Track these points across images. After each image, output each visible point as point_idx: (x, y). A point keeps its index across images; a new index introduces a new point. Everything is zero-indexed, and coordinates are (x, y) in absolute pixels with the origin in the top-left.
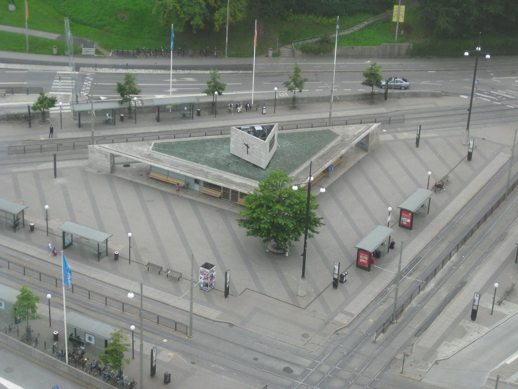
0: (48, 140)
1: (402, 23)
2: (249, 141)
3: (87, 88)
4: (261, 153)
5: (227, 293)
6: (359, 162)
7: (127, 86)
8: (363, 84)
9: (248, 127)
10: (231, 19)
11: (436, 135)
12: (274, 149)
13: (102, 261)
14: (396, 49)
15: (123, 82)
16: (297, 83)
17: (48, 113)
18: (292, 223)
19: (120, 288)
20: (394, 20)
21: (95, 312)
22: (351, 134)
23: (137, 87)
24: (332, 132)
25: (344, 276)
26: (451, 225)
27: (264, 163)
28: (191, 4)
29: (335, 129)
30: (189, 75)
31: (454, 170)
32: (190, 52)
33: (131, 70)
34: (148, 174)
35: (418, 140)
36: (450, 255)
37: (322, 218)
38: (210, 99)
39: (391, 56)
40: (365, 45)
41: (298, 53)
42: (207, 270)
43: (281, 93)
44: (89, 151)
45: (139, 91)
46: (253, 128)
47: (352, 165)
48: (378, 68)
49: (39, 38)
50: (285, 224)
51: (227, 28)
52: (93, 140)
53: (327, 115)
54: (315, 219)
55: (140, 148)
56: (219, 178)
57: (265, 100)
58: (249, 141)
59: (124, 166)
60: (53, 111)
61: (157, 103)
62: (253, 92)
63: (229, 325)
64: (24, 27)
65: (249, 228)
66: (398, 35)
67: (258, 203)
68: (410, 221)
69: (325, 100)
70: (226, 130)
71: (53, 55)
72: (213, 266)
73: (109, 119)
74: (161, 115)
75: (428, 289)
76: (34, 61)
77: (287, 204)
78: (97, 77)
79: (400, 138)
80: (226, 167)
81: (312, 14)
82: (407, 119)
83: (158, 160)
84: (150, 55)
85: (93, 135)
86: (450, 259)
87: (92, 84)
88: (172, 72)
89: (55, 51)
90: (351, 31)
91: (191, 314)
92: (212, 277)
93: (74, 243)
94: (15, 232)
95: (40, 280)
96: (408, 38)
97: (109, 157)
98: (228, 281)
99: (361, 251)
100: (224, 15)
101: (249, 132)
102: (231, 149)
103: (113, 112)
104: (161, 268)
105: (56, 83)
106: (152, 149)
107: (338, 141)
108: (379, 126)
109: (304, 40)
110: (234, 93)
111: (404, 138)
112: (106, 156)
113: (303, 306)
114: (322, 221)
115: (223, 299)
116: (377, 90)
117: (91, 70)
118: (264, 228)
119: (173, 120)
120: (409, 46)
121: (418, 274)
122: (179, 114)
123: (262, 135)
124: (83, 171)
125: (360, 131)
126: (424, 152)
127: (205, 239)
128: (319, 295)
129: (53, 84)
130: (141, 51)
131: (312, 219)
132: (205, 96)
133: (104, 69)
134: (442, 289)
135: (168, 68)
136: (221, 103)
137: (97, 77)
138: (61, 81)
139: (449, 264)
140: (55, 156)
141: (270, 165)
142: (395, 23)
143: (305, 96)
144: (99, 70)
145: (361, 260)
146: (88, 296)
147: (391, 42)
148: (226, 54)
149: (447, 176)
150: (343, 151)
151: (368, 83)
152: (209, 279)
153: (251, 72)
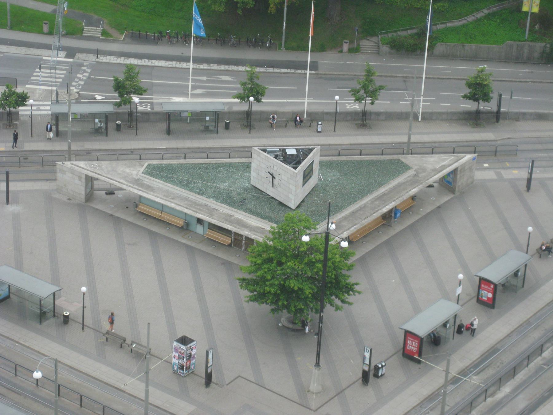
0: (10, 151)
4: (290, 188)
6: (439, 207)
7: (127, 83)
8: (465, 97)
9: (277, 149)
12: (313, 181)
13: (45, 323)
14: (526, 51)
15: (121, 78)
16: (368, 89)
17: (17, 113)
18: (310, 288)
20: (525, 8)
21: (20, 394)
22: (430, 167)
23: (141, 85)
24: (403, 163)
25: (379, 368)
27: (293, 202)
29: (409, 160)
30: (226, 73)
32: (233, 40)
33: (147, 60)
34: (136, 206)
35: (529, 181)
37: (357, 284)
38: (245, 107)
40: (482, 43)
41: (385, 49)
42: (183, 347)
43: (350, 103)
44: (58, 171)
45: (145, 91)
46: (284, 151)
47: (429, 211)
48: (486, 75)
50: (299, 288)
51: (285, 9)
52: (70, 155)
53: (405, 139)
54: (347, 284)
55: (128, 170)
56: (228, 218)
57: (324, 113)
58: (275, 168)
59: (107, 194)
60: (23, 110)
61: (167, 108)
62: (306, 100)
65: (252, 292)
66: (529, 31)
67: (265, 256)
68: (493, 296)
69: (402, 117)
70: (247, 152)
71: (43, 33)
72: (192, 341)
73: (101, 128)
74: (173, 126)
75: (500, 395)
76: (6, 39)
78: (97, 68)
79: (505, 177)
80: (240, 204)
82: (523, 151)
83: (149, 188)
84: (177, 41)
85: (69, 147)
86: (541, 355)
87: (90, 75)
88: (191, 65)
89: (46, 29)
90: (464, 22)
92: (190, 356)
93: (12, 296)
94: (41, 323)
97: (84, 180)
98: (210, 364)
99: (408, 334)
101: (276, 157)
102: (252, 178)
103: (106, 117)
104: (124, 340)
105: (40, 74)
106: (143, 173)
108: (474, 159)
109: (395, 31)
110: (284, 100)
111: (511, 177)
112: (80, 178)
113: (313, 407)
114: (357, 288)
116: (483, 106)
117: (92, 58)
118: (270, 292)
119: (191, 134)
120: (545, 47)
121: (485, 375)
122: (198, 126)
123: (293, 161)
124: (49, 197)
125: (444, 163)
126: (538, 200)
127: (195, 302)
129: (35, 74)
131: (343, 283)
132: (236, 103)
133: (109, 57)
134: (521, 396)
135: (187, 60)
136: (262, 113)
137: (97, 68)
138: (42, 70)
139: (538, 361)
140: (7, 173)
141: (303, 204)
142: (526, 13)
143: (382, 111)
144: (101, 58)
145: (409, 347)
146: (14, 372)
147: (519, 41)
148: (283, 45)
150: (414, 191)
151: (473, 97)
152: (185, 359)
153: (303, 72)
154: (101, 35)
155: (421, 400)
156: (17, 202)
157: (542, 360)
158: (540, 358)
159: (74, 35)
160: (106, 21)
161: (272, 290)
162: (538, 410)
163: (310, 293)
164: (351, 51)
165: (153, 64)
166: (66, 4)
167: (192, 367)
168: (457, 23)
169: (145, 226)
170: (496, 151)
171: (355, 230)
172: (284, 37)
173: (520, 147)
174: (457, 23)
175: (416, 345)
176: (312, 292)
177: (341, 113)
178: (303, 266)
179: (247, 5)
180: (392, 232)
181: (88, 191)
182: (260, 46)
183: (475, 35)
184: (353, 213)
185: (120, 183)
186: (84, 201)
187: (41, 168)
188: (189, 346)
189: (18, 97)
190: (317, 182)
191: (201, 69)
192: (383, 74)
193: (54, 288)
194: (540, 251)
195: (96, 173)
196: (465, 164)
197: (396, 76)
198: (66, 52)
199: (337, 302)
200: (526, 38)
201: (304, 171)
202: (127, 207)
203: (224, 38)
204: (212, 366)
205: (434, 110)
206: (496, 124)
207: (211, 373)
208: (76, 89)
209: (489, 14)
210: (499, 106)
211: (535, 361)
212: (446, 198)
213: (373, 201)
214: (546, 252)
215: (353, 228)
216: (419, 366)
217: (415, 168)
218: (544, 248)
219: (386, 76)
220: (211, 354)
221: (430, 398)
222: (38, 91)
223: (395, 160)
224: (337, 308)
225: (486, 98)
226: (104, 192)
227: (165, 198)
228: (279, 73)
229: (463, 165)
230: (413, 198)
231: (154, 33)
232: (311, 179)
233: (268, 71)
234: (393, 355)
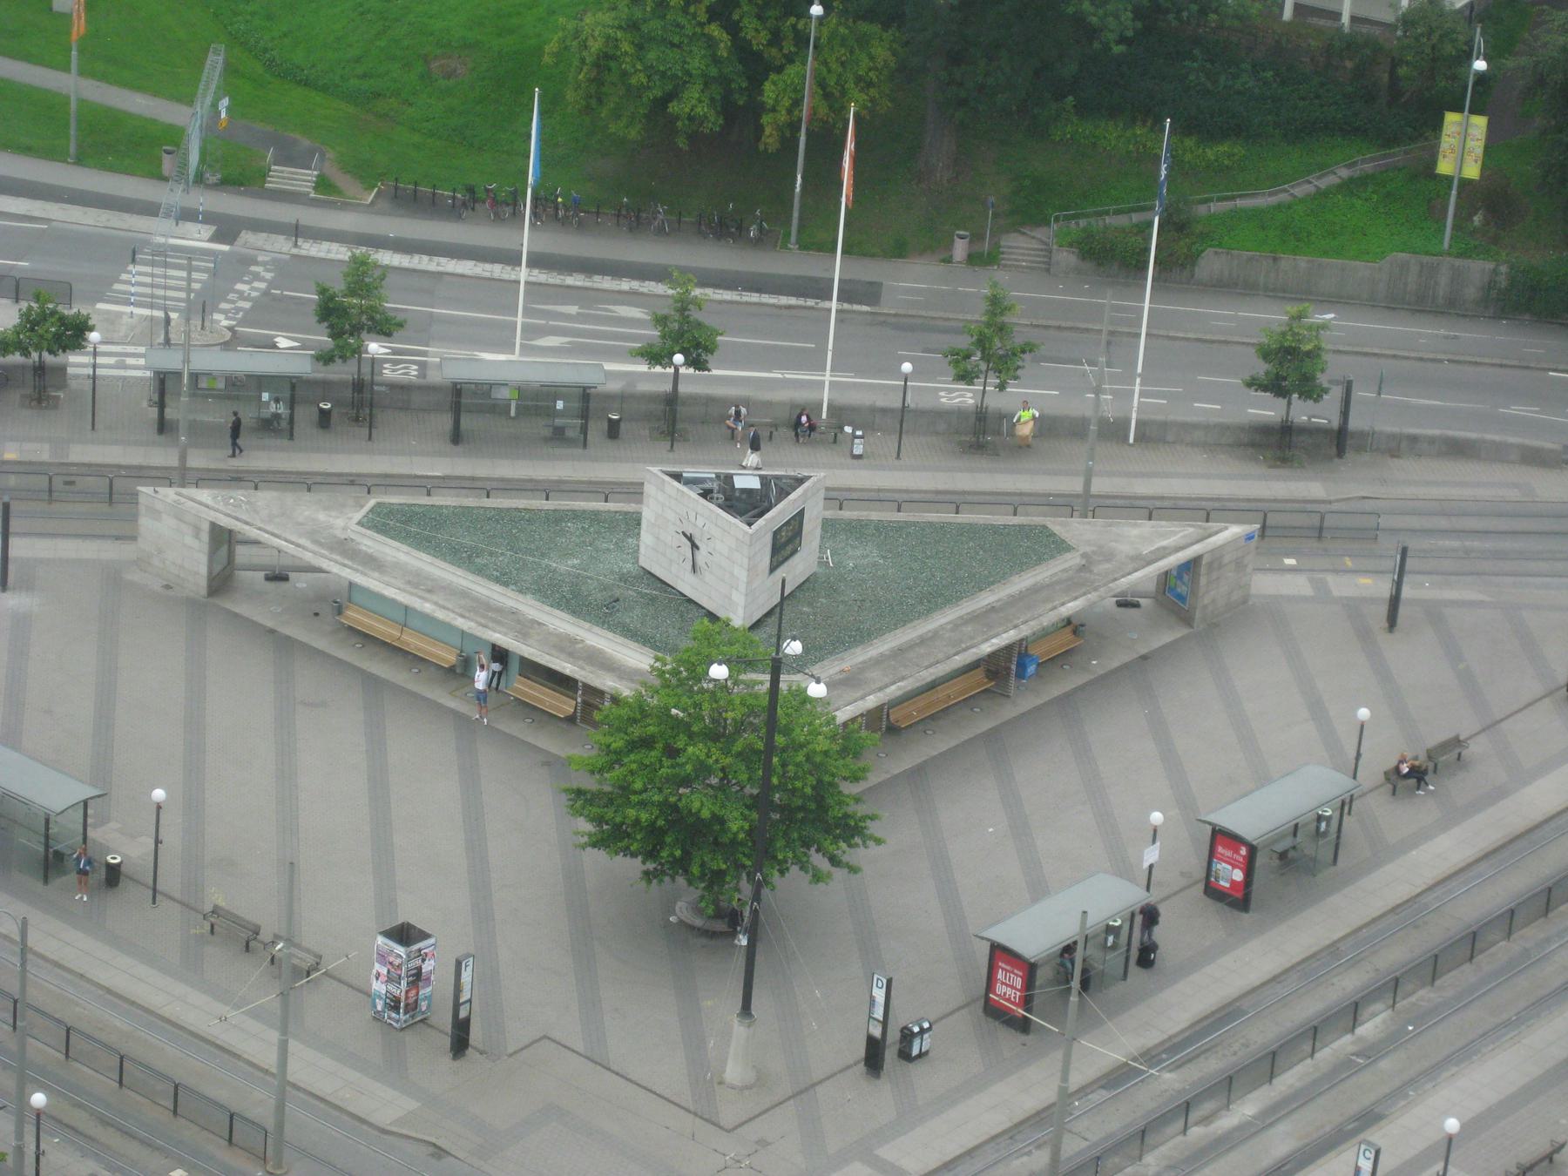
1: (1470, 182)
2: (700, 522)
3: (241, 304)
4: (729, 573)
5: (460, 1041)
6: (1144, 658)
10: (823, 110)
11: (1481, 597)
12: (799, 568)
13: (58, 882)
14: (1443, 280)
15: (338, 286)
16: (993, 350)
17: (61, 370)
18: (745, 818)
19: (89, 981)
20: (1444, 167)
22: (1124, 549)
25: (913, 1035)
26: (1408, 911)
27: (741, 612)
28: (676, 40)
29: (1078, 531)
30: (632, 297)
31: (1503, 725)
32: (660, 217)
33: (425, 258)
35: (1395, 602)
36: (1352, 1012)
37: (873, 818)
39: (1421, 304)
40: (1325, 253)
41: (1066, 258)
42: (400, 950)
44: (142, 509)
45: (401, 325)
46: (729, 479)
47: (1115, 664)
48: (1310, 328)
49: (126, 113)
50: (714, 815)
51: (803, 138)
54: (846, 816)
56: (568, 646)
57: (873, 410)
58: (700, 522)
59: (268, 578)
60: (76, 362)
62: (827, 377)
63: (431, 1149)
64: (66, 69)
66: (1455, 227)
67: (636, 732)
68: (1254, 876)
70: (634, 491)
72: (424, 936)
73: (277, 416)
74: (466, 422)
75: (1226, 1122)
77: (738, 746)
80: (605, 612)
81: (1144, 122)
86: (1352, 1030)
87: (269, 288)
88: (523, 274)
90: (1283, 197)
91: (284, 1088)
92: (417, 977)
94: (46, 880)
95: (175, 1112)
96: (1495, 240)
97: (205, 537)
98: (465, 997)
99: (999, 952)
100: (795, 90)
101: (706, 494)
102: (642, 550)
103: (293, 389)
105: (136, 277)
106: (359, 523)
107: (1065, 570)
108: (1249, 537)
109: (1099, 214)
112: (197, 531)
114: (873, 828)
115: (446, 1060)
116: (1303, 412)
118: (637, 821)
119: (516, 445)
120: (1495, 272)
122: (541, 427)
123: (747, 506)
124: (113, 579)
125: (1164, 543)
126: (1414, 657)
127: (474, 851)
128: (803, 1091)
129: (124, 277)
130: (481, 195)
133: (326, 245)
134: (1282, 1128)
135: (512, 259)
136: (710, 401)
139: (1340, 1046)
142: (1448, 179)
145: (1000, 989)
147: (1427, 253)
148: (793, 238)
149: (1456, 742)
150: (1071, 607)
151: (1276, 386)
154: (315, 188)
155: (1016, 1120)
156: (28, 585)
157: (1353, 1043)
158: (1348, 1038)
159: (242, 184)
160: (330, 155)
161: (644, 816)
162: (1320, 1162)
163: (742, 828)
164: (973, 259)
165: (440, 269)
166: (225, 102)
167: (424, 1005)
168: (1262, 202)
169: (357, 663)
170: (1321, 529)
171: (900, 693)
172: (796, 214)
173: (1384, 521)
174: (1262, 202)
175: (1018, 983)
176: (747, 826)
177: (921, 413)
178: (729, 760)
179: (701, 124)
180: (1009, 711)
181: (218, 568)
182: (731, 235)
183: (1309, 234)
184: (899, 653)
185: (298, 545)
186: (204, 592)
187: (105, 508)
188: (415, 947)
189: (63, 324)
190: (815, 568)
191: (569, 287)
192: (1050, 323)
193: (89, 792)
194: (1394, 777)
195: (237, 519)
196: (1222, 547)
197: (1087, 330)
198: (214, 228)
199: (819, 861)
200: (1446, 245)
201: (776, 533)
202: (316, 614)
203: (639, 211)
204: (470, 1001)
205: (1171, 417)
206: (1336, 460)
207: (467, 1020)
208: (227, 318)
209: (1351, 180)
210: (1345, 414)
211: (1336, 1045)
212: (1167, 637)
213: (956, 625)
214: (1413, 781)
215: (893, 687)
216: (1023, 1038)
217: (1083, 549)
218: (1405, 769)
219: (1059, 328)
220: (470, 969)
221: (1038, 1118)
222: (126, 319)
223: (1032, 528)
224: (817, 877)
225: (1310, 390)
226: (262, 574)
227: (408, 588)
228: (773, 306)
229: (1218, 552)
230: (1071, 625)
231: (454, 191)
232: (797, 557)
233: (745, 299)
234: (959, 1009)
